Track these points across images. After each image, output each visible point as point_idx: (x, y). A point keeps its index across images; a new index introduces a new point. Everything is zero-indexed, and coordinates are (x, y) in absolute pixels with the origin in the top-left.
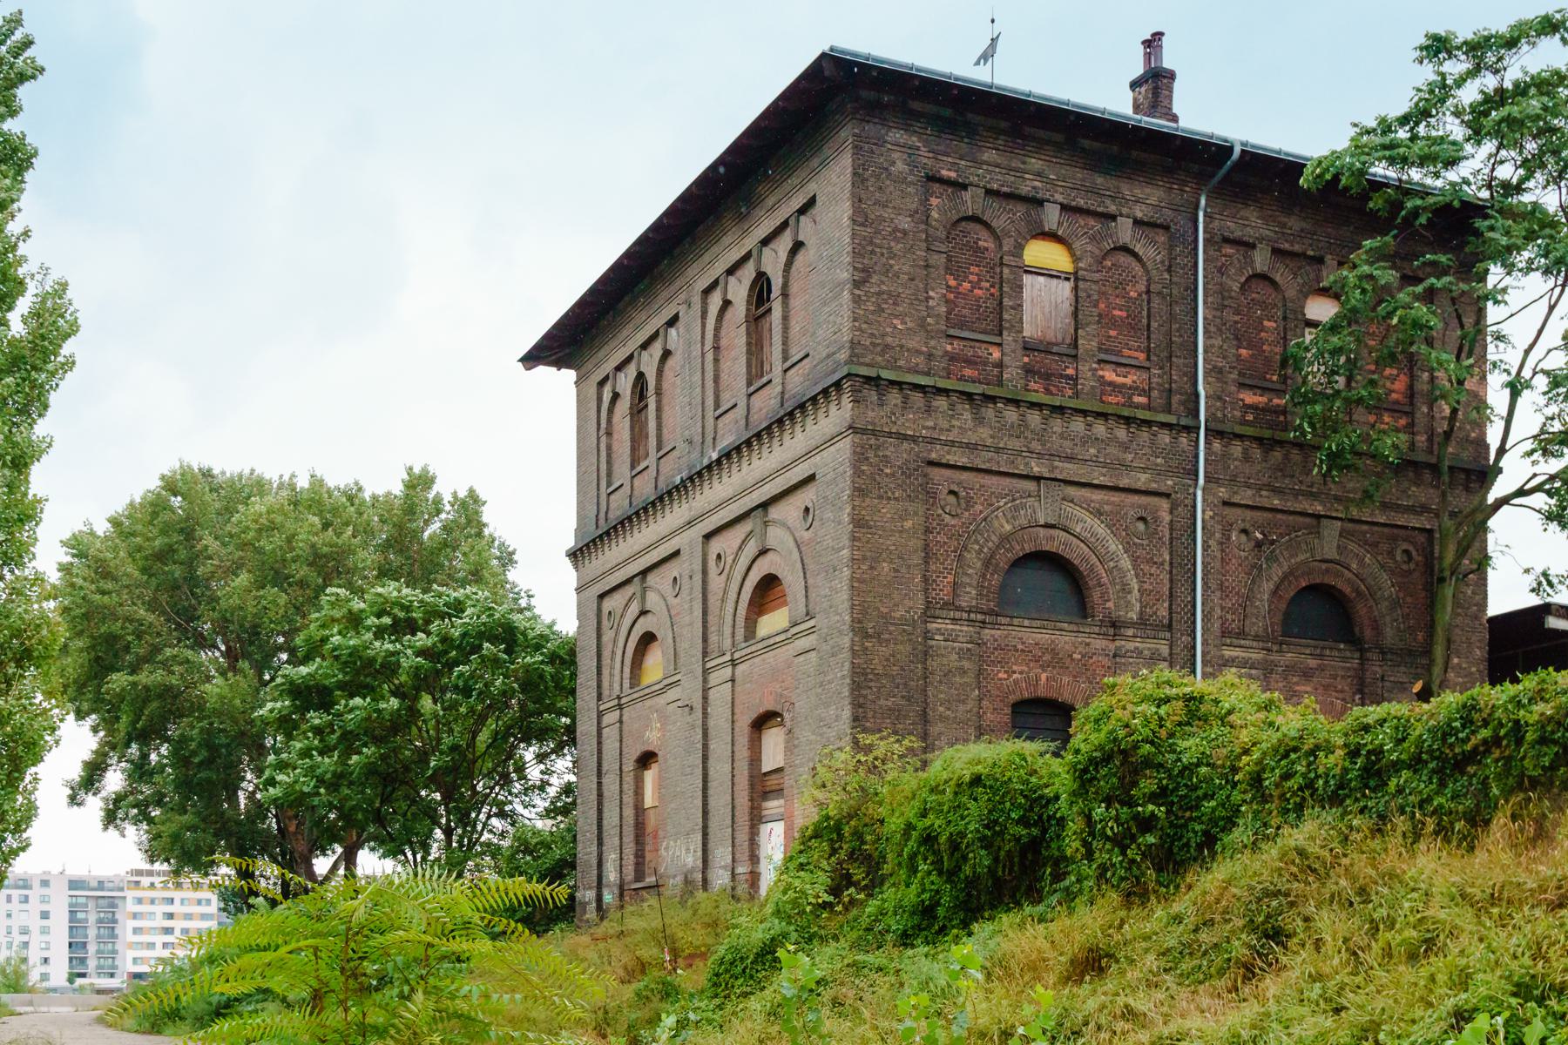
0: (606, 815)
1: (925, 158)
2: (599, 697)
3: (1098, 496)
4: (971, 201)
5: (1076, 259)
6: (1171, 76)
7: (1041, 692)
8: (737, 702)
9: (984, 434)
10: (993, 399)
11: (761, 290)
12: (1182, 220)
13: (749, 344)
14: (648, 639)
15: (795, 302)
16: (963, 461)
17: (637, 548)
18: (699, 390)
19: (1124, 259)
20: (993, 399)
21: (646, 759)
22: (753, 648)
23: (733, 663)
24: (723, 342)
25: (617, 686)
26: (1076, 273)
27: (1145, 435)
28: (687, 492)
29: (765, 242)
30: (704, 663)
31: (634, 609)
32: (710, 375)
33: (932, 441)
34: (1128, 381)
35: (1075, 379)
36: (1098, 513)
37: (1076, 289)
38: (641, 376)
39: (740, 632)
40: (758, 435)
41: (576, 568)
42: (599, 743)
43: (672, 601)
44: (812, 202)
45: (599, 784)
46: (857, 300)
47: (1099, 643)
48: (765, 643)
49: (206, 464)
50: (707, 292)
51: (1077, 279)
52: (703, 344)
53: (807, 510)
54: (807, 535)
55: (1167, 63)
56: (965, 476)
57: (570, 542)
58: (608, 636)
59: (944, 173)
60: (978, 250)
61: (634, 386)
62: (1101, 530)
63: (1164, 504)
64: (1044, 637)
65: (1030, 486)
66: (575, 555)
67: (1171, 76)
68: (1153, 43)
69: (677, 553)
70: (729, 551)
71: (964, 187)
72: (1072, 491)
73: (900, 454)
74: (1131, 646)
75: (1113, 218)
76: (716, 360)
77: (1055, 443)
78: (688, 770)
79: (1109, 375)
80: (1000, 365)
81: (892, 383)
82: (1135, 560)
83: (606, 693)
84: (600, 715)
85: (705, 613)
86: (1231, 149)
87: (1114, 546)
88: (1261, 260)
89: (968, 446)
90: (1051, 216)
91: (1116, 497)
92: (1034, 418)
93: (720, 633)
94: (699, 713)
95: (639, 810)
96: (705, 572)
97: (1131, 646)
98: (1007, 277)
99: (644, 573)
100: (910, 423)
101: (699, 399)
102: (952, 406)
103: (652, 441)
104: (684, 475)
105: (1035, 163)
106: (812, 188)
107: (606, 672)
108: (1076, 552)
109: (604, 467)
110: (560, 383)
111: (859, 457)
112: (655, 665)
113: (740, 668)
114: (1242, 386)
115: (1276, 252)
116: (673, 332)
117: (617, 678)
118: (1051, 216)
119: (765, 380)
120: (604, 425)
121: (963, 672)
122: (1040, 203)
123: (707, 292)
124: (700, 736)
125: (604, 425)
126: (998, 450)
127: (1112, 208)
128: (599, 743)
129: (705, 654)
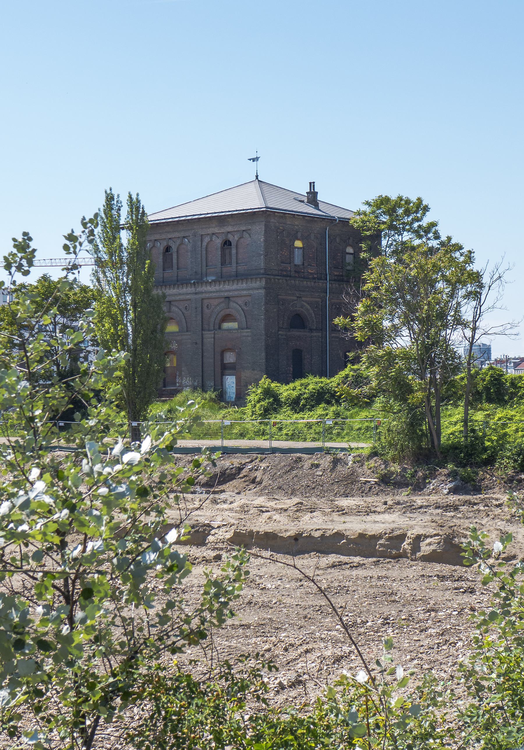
5: (303, 244)
26: (303, 247)
32: (204, 259)
46: (266, 259)
64: (298, 333)
79: (310, 271)
111: (267, 294)
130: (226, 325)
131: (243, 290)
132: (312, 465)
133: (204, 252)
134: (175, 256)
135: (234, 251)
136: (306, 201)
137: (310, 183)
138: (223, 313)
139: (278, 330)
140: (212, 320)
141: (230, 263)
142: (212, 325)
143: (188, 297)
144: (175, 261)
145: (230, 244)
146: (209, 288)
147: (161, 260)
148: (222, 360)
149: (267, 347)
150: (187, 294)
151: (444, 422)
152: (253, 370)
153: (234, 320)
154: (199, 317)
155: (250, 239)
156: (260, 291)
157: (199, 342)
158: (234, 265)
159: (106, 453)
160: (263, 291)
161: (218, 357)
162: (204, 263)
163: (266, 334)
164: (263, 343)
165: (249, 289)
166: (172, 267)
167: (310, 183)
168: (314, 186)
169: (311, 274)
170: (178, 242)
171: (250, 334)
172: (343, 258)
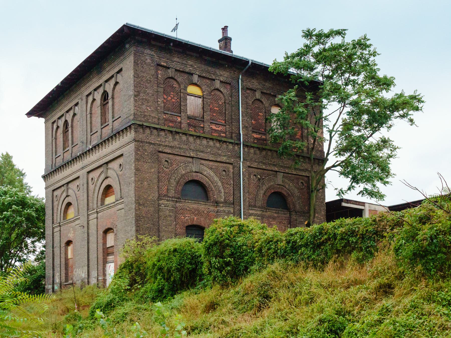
0: (55, 261)
1: (156, 58)
2: (53, 223)
3: (211, 163)
4: (171, 73)
8: (98, 225)
9: (176, 143)
11: (105, 96)
13: (101, 113)
14: (69, 204)
15: (116, 100)
16: (169, 151)
17: (65, 175)
18: (85, 126)
21: (69, 243)
22: (104, 208)
23: (97, 212)
24: (93, 112)
25: (59, 219)
26: (203, 96)
27: (225, 145)
28: (82, 158)
29: (106, 81)
30: (88, 212)
31: (65, 195)
33: (160, 145)
34: (219, 129)
35: (203, 128)
36: (211, 169)
37: (203, 101)
38: (66, 121)
39: (99, 203)
40: (105, 141)
41: (45, 181)
42: (53, 238)
43: (77, 192)
44: (121, 70)
45: (53, 251)
47: (212, 208)
48: (108, 206)
50: (88, 96)
51: (203, 98)
52: (86, 112)
53: (120, 165)
54: (120, 173)
56: (170, 156)
57: (43, 173)
58: (56, 203)
59: (162, 63)
60: (172, 87)
61: (64, 124)
62: (212, 174)
63: (231, 167)
64: (195, 206)
65: (190, 160)
66: (44, 177)
67: (230, 39)
69: (78, 177)
70: (95, 177)
71: (169, 68)
72: (203, 162)
73: (150, 149)
74: (222, 209)
75: (214, 80)
76: (91, 117)
78: (82, 247)
80: (180, 123)
81: (147, 127)
82: (222, 183)
83: (55, 221)
84: (53, 229)
85: (88, 196)
86: (248, 62)
87: (216, 179)
88: (258, 95)
90: (195, 78)
93: (93, 203)
95: (67, 259)
96: (88, 183)
97: (222, 209)
98: (182, 97)
99: (68, 183)
100: (152, 139)
101: (85, 129)
102: (166, 134)
103: (70, 142)
104: (81, 153)
105: (190, 62)
106: (121, 66)
107: (55, 215)
108: (204, 180)
109: (54, 149)
110: (39, 123)
111: (137, 149)
112: (71, 213)
113: (99, 214)
114: (253, 132)
115: (262, 93)
116: (77, 108)
117: (59, 217)
118: (195, 78)
119: (106, 124)
120: (54, 136)
121: (170, 216)
122: (192, 74)
123: (88, 96)
124: (86, 236)
125: (54, 136)
126: (180, 148)
127: (214, 77)
128: (53, 238)
129: (88, 209)
130: (110, 200)
133: (89, 116)
164: (134, 214)
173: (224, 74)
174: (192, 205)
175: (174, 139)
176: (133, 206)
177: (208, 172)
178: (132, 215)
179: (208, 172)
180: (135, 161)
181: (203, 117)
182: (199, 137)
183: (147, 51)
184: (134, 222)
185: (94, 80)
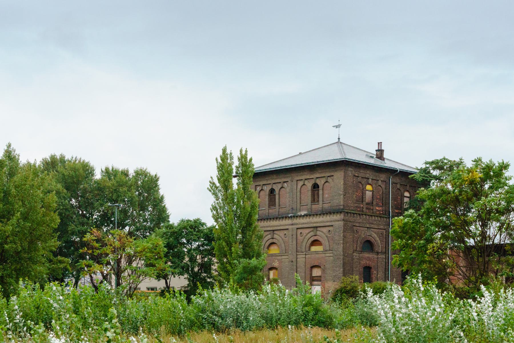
1: (353, 172)
3: (375, 230)
4: (359, 179)
6: (383, 151)
7: (367, 265)
9: (361, 220)
10: (362, 214)
12: (388, 181)
15: (326, 192)
16: (358, 225)
17: (271, 225)
19: (380, 187)
20: (362, 214)
24: (302, 191)
32: (298, 198)
33: (354, 222)
35: (373, 209)
36: (376, 233)
37: (373, 193)
46: (344, 198)
49: (47, 156)
55: (383, 149)
56: (358, 228)
62: (376, 236)
63: (384, 231)
67: (383, 151)
68: (380, 144)
72: (372, 229)
73: (350, 224)
77: (371, 221)
79: (377, 208)
87: (378, 239)
88: (398, 186)
89: (359, 223)
90: (370, 180)
91: (378, 230)
92: (368, 217)
94: (295, 263)
105: (368, 172)
108: (372, 240)
111: (345, 225)
113: (307, 256)
115: (401, 185)
118: (370, 180)
130: (314, 249)
131: (328, 222)
132: (227, 198)
133: (299, 193)
134: (277, 197)
135: (321, 192)
136: (375, 157)
137: (379, 143)
138: (312, 239)
139: (353, 253)
140: (304, 244)
141: (318, 201)
142: (304, 248)
143: (287, 227)
144: (277, 200)
145: (318, 187)
146: (302, 220)
147: (267, 199)
148: (311, 274)
149: (344, 264)
150: (286, 225)
151: (39, 285)
152: (334, 281)
153: (320, 244)
154: (295, 242)
155: (333, 183)
156: (340, 222)
157: (294, 260)
158: (321, 202)
159: (304, 320)
160: (342, 223)
161: (308, 272)
162: (299, 202)
163: (344, 255)
165: (331, 221)
166: (275, 205)
167: (379, 143)
168: (381, 145)
169: (379, 210)
170: (280, 186)
171: (331, 255)
172: (402, 200)
173: (383, 177)
174: (366, 255)
175: (360, 218)
176: (342, 257)
177: (375, 235)
178: (340, 262)
179: (375, 235)
180: (343, 232)
181: (373, 203)
182: (371, 216)
183: (350, 169)
184: (342, 266)
185: (306, 173)
